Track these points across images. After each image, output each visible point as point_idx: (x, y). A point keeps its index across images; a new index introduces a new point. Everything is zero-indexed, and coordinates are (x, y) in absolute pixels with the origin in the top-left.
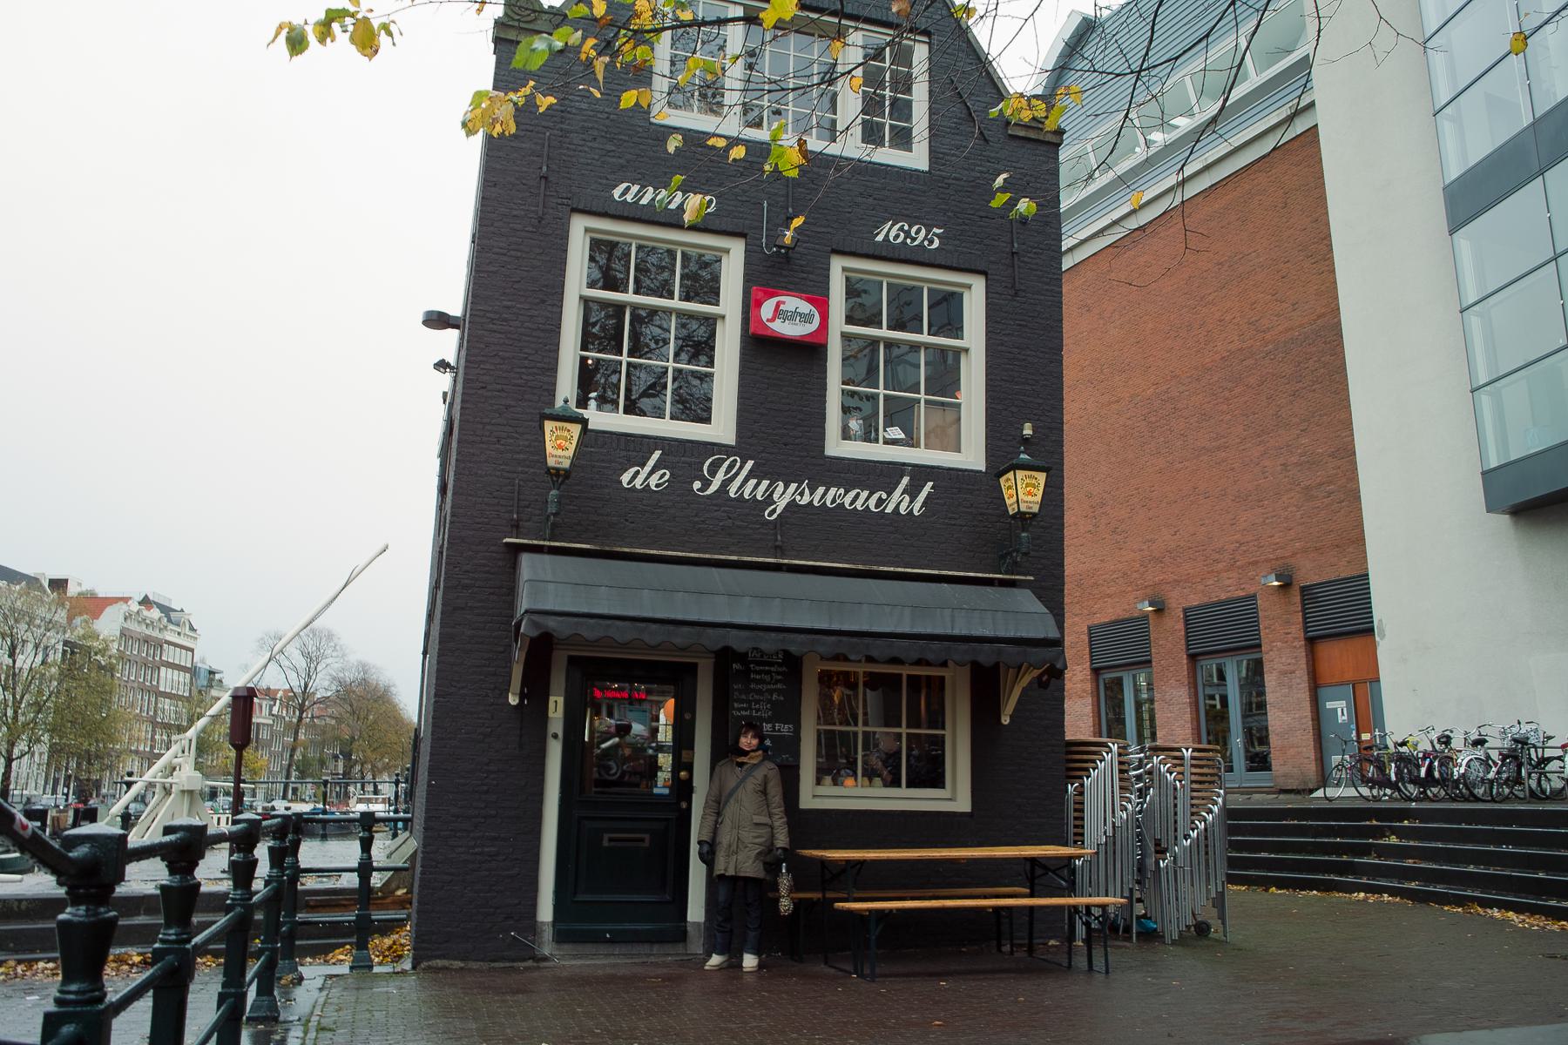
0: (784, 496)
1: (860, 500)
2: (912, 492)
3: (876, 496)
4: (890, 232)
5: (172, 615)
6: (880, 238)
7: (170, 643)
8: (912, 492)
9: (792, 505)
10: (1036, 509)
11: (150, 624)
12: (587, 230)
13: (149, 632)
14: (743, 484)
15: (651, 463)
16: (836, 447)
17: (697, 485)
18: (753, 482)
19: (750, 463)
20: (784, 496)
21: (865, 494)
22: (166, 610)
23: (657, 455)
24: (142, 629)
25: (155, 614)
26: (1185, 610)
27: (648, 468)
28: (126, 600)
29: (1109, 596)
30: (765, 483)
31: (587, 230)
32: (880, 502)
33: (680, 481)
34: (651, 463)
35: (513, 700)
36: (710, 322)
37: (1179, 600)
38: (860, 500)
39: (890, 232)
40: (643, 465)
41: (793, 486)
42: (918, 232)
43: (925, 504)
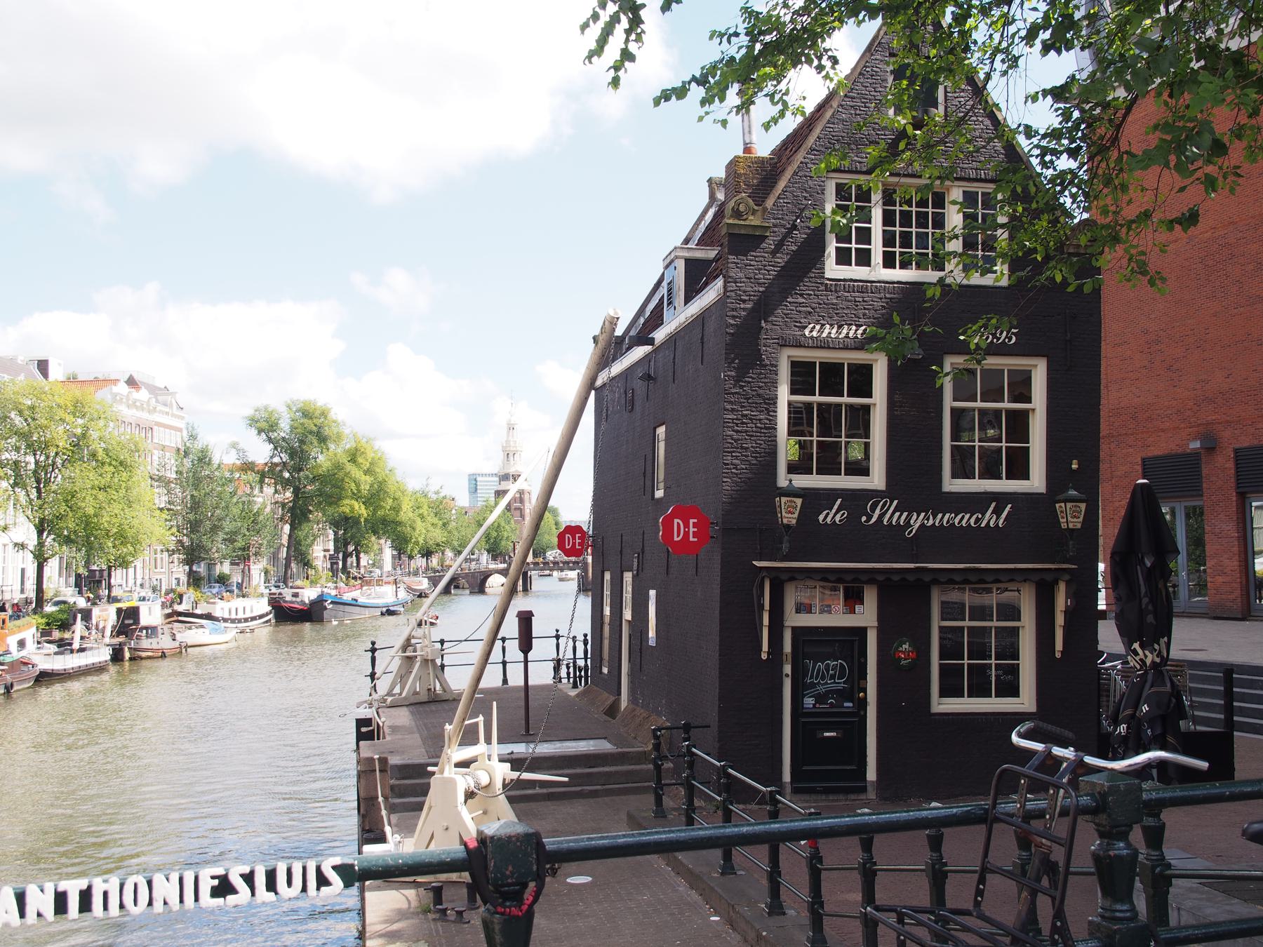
0: (917, 521)
1: (965, 520)
2: (997, 512)
8: (997, 512)
9: (922, 525)
10: (1079, 526)
14: (894, 516)
15: (836, 507)
16: (953, 485)
17: (864, 519)
18: (897, 514)
20: (917, 521)
21: (967, 516)
26: (1236, 451)
29: (1163, 431)
30: (905, 514)
32: (977, 520)
33: (853, 519)
34: (836, 507)
35: (605, 670)
36: (866, 409)
37: (1236, 438)
38: (965, 520)
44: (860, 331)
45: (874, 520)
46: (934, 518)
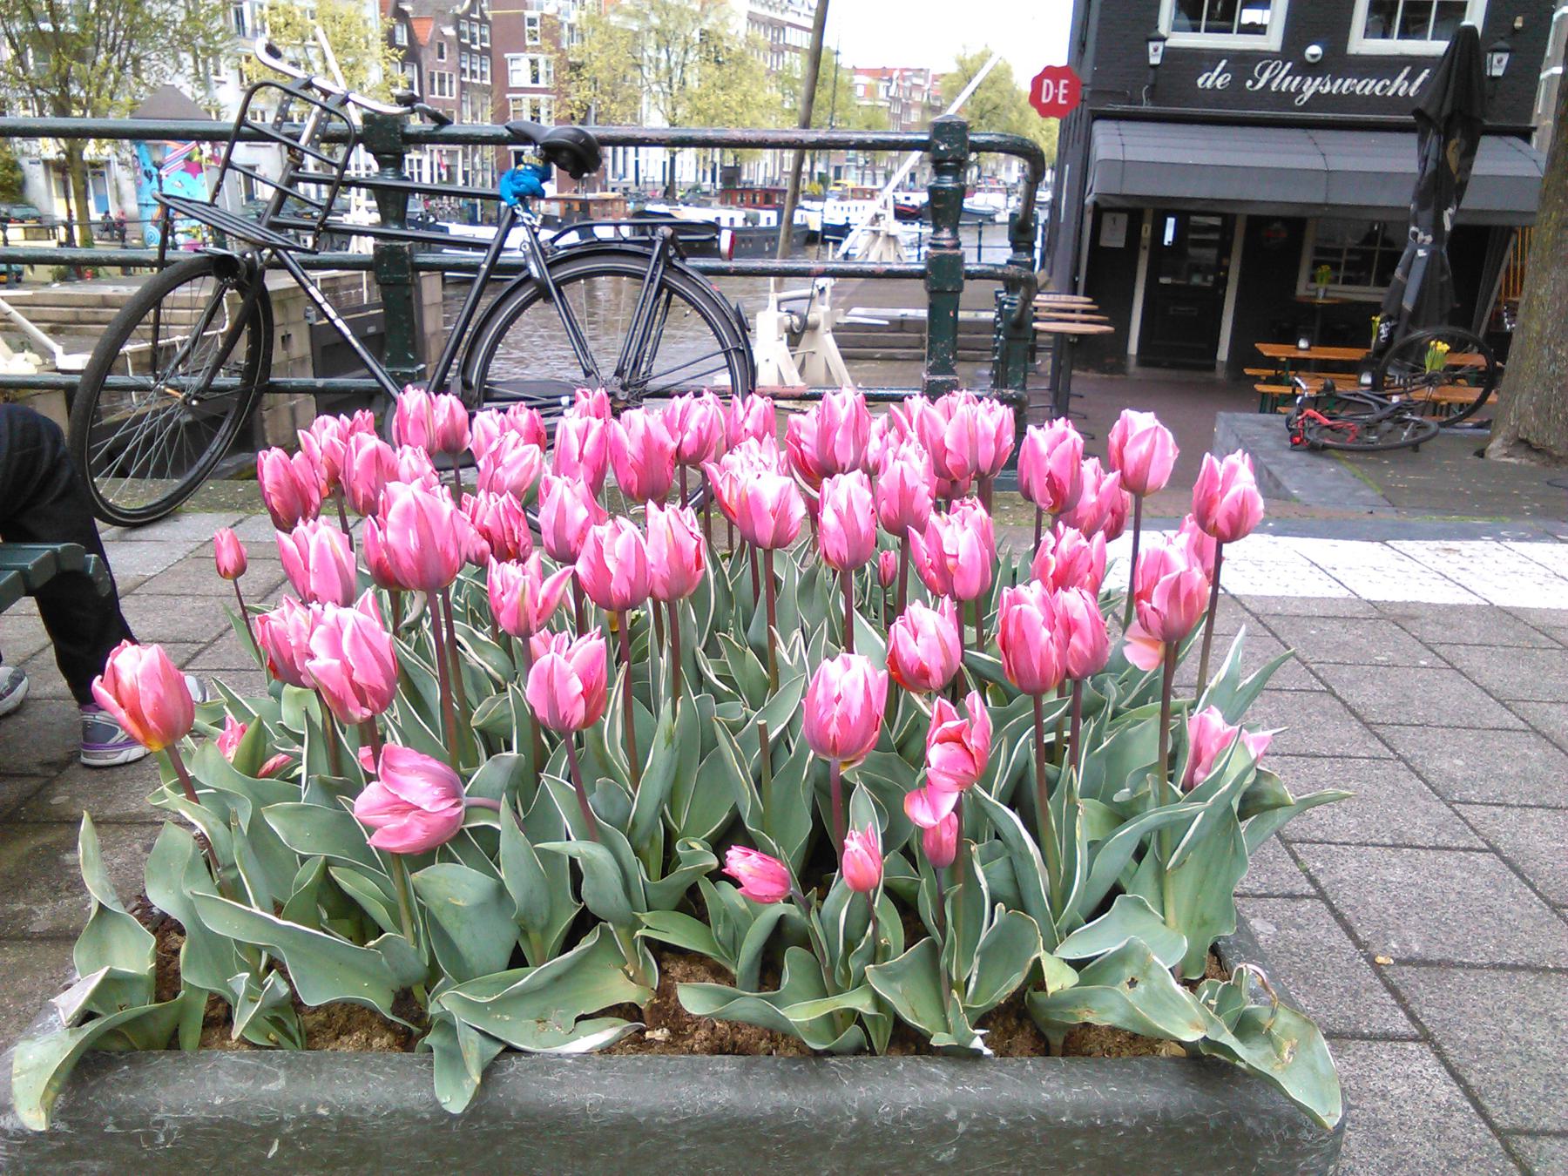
1: (1370, 87)
2: (1411, 78)
8: (1411, 78)
9: (1317, 93)
14: (1282, 79)
15: (1219, 69)
17: (1249, 83)
19: (1289, 65)
23: (1223, 63)
32: (1385, 87)
33: (1237, 83)
34: (1219, 69)
38: (1370, 87)
41: (1319, 80)
45: (1260, 85)
46: (1332, 84)
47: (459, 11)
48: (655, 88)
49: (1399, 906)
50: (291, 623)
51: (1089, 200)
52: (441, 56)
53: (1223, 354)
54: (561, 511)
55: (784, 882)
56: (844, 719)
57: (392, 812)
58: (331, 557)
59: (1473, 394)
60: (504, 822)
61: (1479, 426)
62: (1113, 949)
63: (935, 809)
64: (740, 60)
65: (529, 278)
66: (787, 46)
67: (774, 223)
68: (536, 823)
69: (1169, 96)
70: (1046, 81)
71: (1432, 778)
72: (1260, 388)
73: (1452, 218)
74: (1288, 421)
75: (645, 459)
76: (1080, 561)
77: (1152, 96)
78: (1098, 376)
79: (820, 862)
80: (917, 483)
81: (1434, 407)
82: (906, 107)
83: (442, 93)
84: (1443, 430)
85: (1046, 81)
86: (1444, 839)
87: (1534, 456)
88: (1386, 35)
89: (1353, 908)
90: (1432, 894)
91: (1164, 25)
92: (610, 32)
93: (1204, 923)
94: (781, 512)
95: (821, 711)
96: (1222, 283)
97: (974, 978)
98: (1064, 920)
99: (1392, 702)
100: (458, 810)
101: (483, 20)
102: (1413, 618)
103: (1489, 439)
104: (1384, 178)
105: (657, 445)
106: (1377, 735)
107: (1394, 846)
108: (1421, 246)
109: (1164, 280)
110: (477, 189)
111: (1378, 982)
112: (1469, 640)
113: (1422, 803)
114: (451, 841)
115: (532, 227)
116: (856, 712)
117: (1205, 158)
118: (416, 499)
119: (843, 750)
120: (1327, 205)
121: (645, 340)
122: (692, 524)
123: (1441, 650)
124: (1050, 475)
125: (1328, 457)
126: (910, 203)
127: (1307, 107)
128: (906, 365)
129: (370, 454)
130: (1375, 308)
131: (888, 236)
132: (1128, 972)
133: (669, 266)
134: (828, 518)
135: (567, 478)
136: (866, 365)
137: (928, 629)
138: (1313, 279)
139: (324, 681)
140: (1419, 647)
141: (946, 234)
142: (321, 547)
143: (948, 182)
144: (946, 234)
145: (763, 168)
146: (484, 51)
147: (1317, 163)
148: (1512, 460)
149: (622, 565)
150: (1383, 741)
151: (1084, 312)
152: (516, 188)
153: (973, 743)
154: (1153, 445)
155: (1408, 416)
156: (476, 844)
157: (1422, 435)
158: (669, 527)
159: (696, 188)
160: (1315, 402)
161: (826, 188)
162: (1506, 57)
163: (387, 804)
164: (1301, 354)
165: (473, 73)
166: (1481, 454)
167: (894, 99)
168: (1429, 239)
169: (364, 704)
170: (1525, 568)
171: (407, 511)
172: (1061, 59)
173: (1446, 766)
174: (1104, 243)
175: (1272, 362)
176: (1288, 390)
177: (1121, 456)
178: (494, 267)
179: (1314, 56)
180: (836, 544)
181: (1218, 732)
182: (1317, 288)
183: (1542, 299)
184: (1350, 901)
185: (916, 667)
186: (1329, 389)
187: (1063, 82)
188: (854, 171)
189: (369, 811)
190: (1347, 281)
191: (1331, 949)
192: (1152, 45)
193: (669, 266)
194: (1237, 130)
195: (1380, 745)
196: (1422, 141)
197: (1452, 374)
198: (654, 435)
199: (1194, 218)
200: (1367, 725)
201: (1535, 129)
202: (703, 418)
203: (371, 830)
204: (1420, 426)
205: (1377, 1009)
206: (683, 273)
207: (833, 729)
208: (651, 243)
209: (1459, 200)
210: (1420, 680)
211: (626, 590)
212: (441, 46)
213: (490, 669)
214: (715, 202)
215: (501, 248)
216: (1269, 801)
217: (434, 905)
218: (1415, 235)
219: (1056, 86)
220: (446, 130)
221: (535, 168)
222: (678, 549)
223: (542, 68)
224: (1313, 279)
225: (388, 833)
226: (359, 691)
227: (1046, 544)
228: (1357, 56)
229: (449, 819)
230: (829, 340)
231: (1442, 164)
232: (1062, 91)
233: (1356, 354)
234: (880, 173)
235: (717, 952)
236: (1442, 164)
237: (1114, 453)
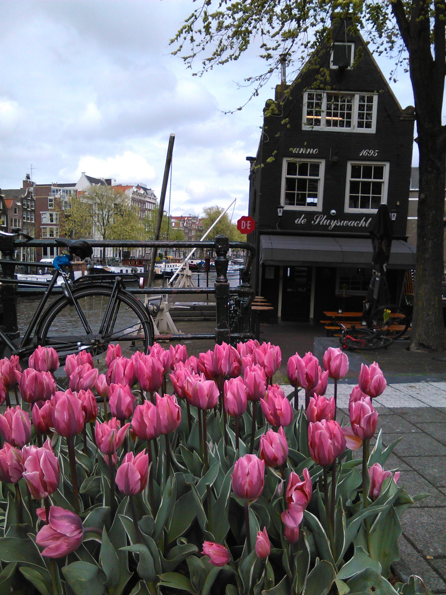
1: (353, 224)
2: (366, 221)
3: (356, 222)
4: (364, 153)
5: (148, 191)
6: (361, 155)
7: (147, 202)
8: (366, 221)
9: (336, 225)
11: (141, 195)
12: (287, 161)
13: (141, 198)
14: (324, 221)
15: (302, 218)
17: (313, 222)
19: (325, 216)
21: (354, 222)
22: (145, 189)
23: (303, 216)
24: (138, 197)
25: (142, 191)
27: (301, 219)
28: (132, 187)
30: (329, 221)
31: (287, 161)
32: (358, 224)
33: (309, 222)
34: (302, 218)
38: (353, 224)
39: (364, 153)
40: (300, 218)
41: (336, 221)
42: (371, 152)
43: (369, 224)
44: (314, 151)
45: (316, 223)
46: (340, 222)
47: (23, 196)
48: (98, 224)
49: (429, 533)
50: (8, 454)
51: (261, 262)
52: (15, 212)
53: (312, 316)
54: (120, 399)
55: (228, 556)
56: (251, 482)
57: (52, 539)
58: (22, 424)
59: (403, 327)
60: (104, 541)
61: (406, 339)
62: (359, 572)
63: (295, 520)
64: (130, 215)
65: (65, 297)
66: (146, 209)
67: (143, 272)
68: (117, 539)
69: (286, 226)
70: (243, 222)
71: (428, 477)
72: (327, 328)
73: (386, 267)
74: (340, 340)
75: (152, 375)
76: (327, 409)
77: (280, 226)
78: (267, 325)
79: (236, 542)
80: (260, 380)
81: (388, 333)
82: (190, 230)
83: (15, 226)
84: (395, 341)
85: (243, 222)
86: (438, 503)
87: (426, 349)
88: (356, 207)
89: (413, 536)
90: (440, 527)
91: (282, 204)
92: (81, 204)
93: (385, 555)
94: (211, 396)
95: (241, 480)
96: (309, 290)
97: (304, 591)
98: (338, 563)
99: (406, 447)
100: (81, 534)
101: (32, 200)
102: (406, 414)
103: (410, 344)
104: (361, 254)
105: (156, 370)
106: (404, 461)
107: (421, 507)
108: (377, 276)
109: (289, 290)
110: (29, 262)
111: (429, 567)
112: (427, 421)
113: (427, 488)
114: (76, 551)
115: (66, 277)
116: (255, 480)
117: (301, 247)
118: (68, 398)
119: (248, 496)
120: (343, 263)
121: (111, 318)
122: (176, 402)
123: (418, 425)
124: (307, 374)
125: (356, 352)
126: (193, 264)
127: (334, 229)
128: (197, 323)
129: (33, 377)
130: (363, 298)
131: (187, 276)
132: (370, 584)
133: (120, 291)
134: (229, 395)
135: (120, 385)
136: (181, 323)
137: (275, 441)
138: (341, 288)
139: (31, 481)
140: (410, 425)
141: (222, 277)
142: (17, 418)
143: (222, 259)
144: (222, 277)
145: (137, 253)
146: (32, 211)
147: (338, 249)
148: (419, 351)
149: (151, 421)
150: (407, 463)
151: (261, 302)
152: (59, 263)
153: (307, 489)
154: (341, 360)
155: (382, 336)
156: (93, 551)
157: (387, 343)
158: (167, 403)
159: (113, 259)
160: (347, 333)
161: (161, 259)
162: (396, 214)
163: (51, 535)
164: (340, 315)
165: (28, 219)
166: (408, 349)
167: (185, 227)
168: (379, 274)
169: (46, 490)
170: (439, 392)
171: (64, 402)
172: (246, 213)
173: (431, 472)
174: (266, 277)
175: (330, 318)
176: (339, 328)
177: (329, 366)
178: (51, 293)
179: (333, 213)
180: (233, 407)
181: (381, 473)
182: (342, 292)
183: (421, 295)
184: (411, 533)
185: (273, 456)
186: (353, 328)
187: (248, 222)
188: (172, 253)
189: (43, 540)
190: (352, 289)
191: (409, 554)
192: (279, 210)
193: (120, 291)
194: (320, 238)
195: (406, 465)
196: (373, 242)
197: (392, 321)
198: (155, 365)
199: (296, 268)
200: (399, 457)
201: (408, 237)
202: (165, 355)
203: (42, 548)
204: (386, 340)
205: (432, 580)
206: (125, 293)
207: (246, 487)
208: (113, 283)
209: (388, 262)
210: (414, 438)
211: (153, 431)
212: (16, 209)
213: (84, 466)
214: (121, 264)
215: (52, 286)
216: (403, 501)
217: (71, 581)
218: (375, 273)
219: (246, 223)
220: (31, 242)
221: (67, 255)
222: (171, 413)
223: (54, 217)
224: (341, 288)
225: (50, 549)
226: (44, 484)
227: (312, 402)
228: (348, 214)
229: (78, 539)
230: (168, 314)
231: (381, 249)
232: (248, 225)
233: (359, 314)
234: (182, 253)
235: (193, 589)
236: (381, 249)
237: (326, 363)
